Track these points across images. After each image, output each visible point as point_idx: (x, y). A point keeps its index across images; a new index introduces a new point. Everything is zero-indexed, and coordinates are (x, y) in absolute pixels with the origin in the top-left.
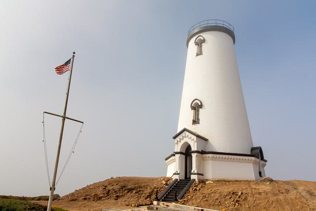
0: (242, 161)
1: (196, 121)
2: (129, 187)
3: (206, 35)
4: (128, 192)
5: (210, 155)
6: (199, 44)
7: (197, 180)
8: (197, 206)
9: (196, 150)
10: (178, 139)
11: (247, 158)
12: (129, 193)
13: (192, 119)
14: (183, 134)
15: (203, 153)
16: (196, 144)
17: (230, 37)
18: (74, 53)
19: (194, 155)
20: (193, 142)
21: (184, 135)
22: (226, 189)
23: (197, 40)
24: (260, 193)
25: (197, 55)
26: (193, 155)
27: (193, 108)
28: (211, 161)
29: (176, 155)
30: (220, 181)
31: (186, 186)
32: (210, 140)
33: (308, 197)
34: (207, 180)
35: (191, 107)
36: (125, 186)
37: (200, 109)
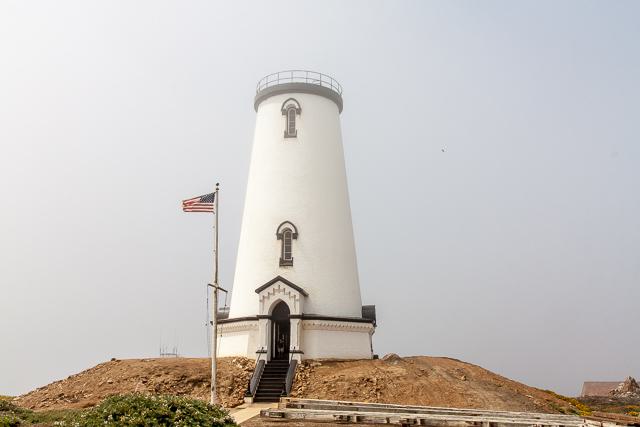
0: (351, 330)
1: (286, 261)
2: (193, 377)
3: (305, 100)
4: (194, 386)
5: (317, 322)
6: (291, 113)
7: (300, 362)
8: (343, 398)
9: (298, 313)
10: (265, 293)
11: (360, 324)
12: (196, 388)
13: (279, 256)
14: (275, 286)
15: (303, 317)
16: (298, 304)
17: (324, 99)
18: (218, 184)
19: (294, 324)
20: (292, 300)
21: (276, 288)
22: (357, 373)
23: (286, 105)
24: (398, 378)
25: (287, 136)
26: (291, 320)
27: (280, 236)
28: (316, 332)
29: (261, 320)
30: (354, 361)
31: (288, 374)
32: (310, 296)
33: (450, 379)
34: (312, 361)
35: (277, 234)
36: (184, 377)
37: (294, 241)
